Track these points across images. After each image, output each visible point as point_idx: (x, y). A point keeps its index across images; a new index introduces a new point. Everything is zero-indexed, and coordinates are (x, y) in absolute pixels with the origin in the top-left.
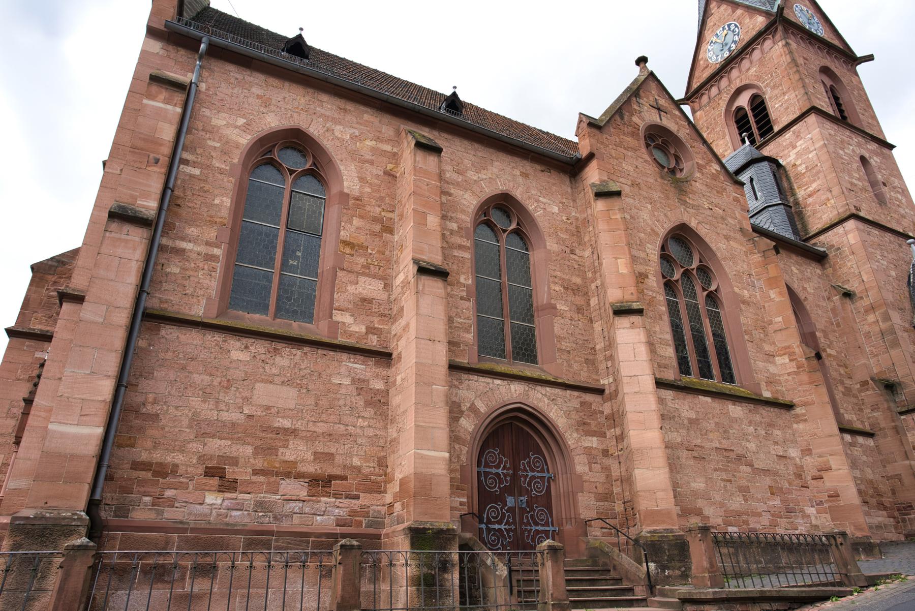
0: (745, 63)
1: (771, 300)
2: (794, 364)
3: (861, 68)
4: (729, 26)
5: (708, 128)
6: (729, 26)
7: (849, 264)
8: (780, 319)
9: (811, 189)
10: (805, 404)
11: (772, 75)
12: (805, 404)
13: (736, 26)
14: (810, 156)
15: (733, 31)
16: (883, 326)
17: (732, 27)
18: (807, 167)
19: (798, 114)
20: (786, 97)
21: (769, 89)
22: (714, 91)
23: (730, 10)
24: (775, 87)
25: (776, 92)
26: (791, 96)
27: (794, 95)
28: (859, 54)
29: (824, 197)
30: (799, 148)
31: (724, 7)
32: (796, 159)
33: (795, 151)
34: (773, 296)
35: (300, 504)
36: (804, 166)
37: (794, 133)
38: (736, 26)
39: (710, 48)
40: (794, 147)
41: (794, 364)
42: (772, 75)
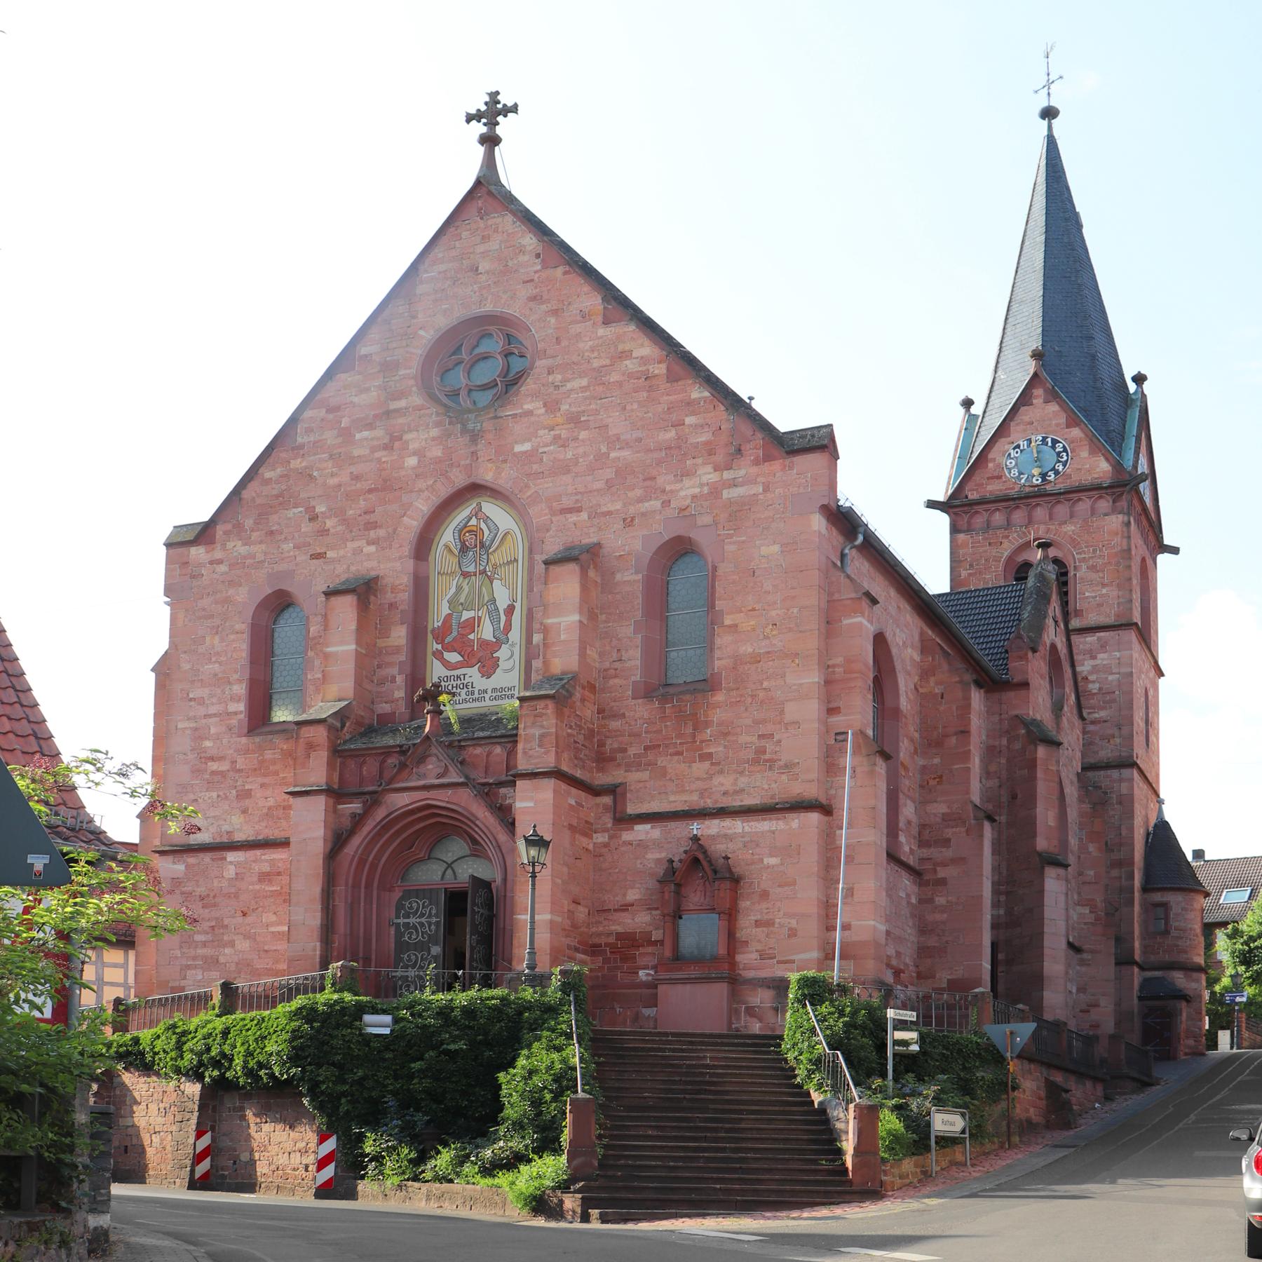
0: (1062, 510)
1: (1090, 853)
2: (1093, 915)
3: (1162, 559)
4: (1055, 442)
5: (971, 566)
6: (1055, 442)
7: (1112, 813)
8: (1092, 873)
9: (1097, 715)
10: (1092, 952)
11: (1094, 551)
12: (1092, 952)
13: (1065, 450)
14: (1110, 678)
15: (1058, 454)
16: (1124, 882)
17: (1059, 448)
18: (1100, 689)
19: (1110, 620)
20: (1104, 591)
21: (1084, 567)
22: (998, 518)
23: (1062, 419)
24: (1093, 568)
25: (1094, 576)
26: (1111, 592)
27: (1115, 593)
28: (1167, 541)
29: (1109, 732)
30: (1098, 662)
31: (1053, 407)
32: (1091, 673)
33: (1092, 662)
34: (1091, 849)
35: (168, 926)
36: (1097, 685)
37: (1099, 639)
38: (1065, 450)
39: (1013, 454)
40: (1094, 658)
41: (1093, 915)
42: (1094, 551)
